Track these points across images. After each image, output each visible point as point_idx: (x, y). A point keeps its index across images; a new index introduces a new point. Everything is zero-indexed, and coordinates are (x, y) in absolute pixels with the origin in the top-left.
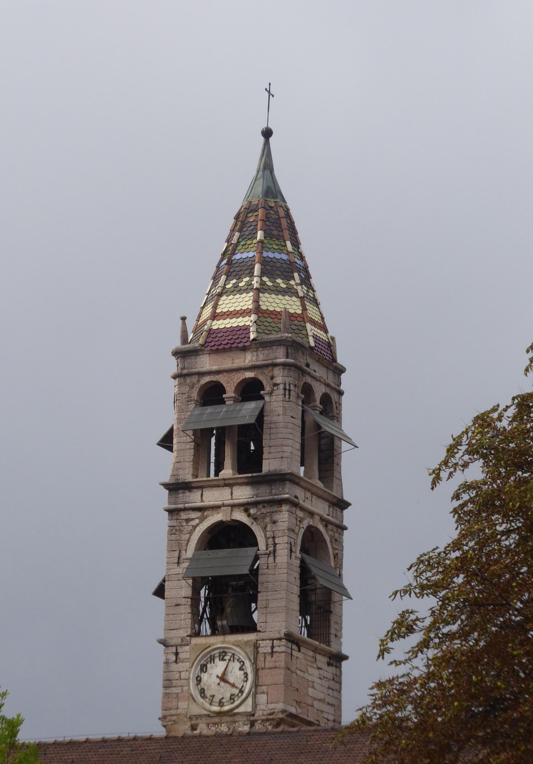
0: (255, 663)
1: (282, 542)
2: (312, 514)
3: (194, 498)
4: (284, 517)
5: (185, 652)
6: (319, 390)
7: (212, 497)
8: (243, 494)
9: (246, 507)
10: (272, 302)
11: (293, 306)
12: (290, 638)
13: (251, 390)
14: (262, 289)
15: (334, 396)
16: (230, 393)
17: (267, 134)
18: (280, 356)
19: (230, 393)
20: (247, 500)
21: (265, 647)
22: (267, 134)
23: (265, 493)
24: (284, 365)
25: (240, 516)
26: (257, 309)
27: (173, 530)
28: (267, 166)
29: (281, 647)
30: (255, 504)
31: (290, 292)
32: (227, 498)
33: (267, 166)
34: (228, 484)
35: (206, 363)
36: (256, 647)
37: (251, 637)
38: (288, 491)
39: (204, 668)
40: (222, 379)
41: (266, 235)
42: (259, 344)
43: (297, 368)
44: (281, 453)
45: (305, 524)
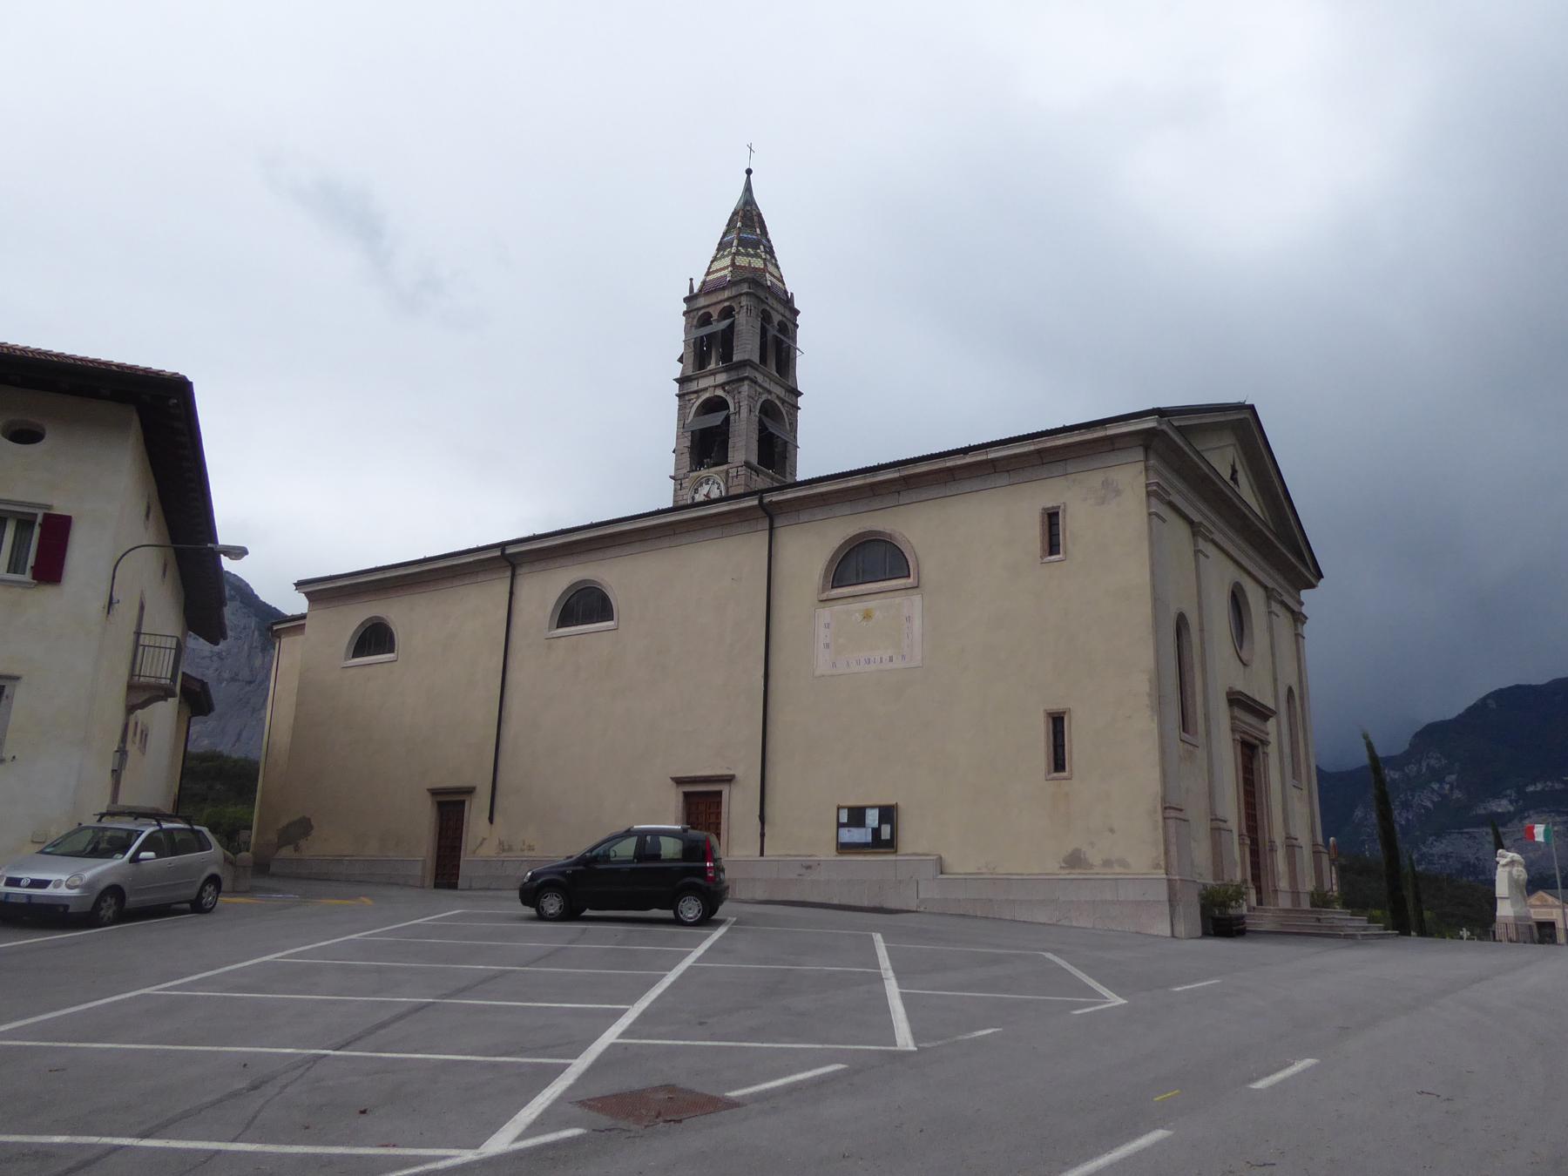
0: (726, 483)
1: (744, 404)
2: (770, 392)
3: (694, 386)
4: (745, 388)
5: (686, 483)
6: (776, 318)
7: (703, 383)
8: (721, 378)
9: (722, 386)
10: (742, 261)
11: (758, 263)
12: (747, 464)
13: (727, 313)
14: (737, 253)
15: (790, 326)
16: (715, 316)
17: (749, 172)
18: (745, 288)
19: (715, 316)
20: (1279, 839)
21: (733, 472)
22: (749, 172)
23: (734, 375)
24: (747, 294)
25: (720, 392)
26: (733, 264)
27: (681, 408)
28: (748, 189)
29: (742, 471)
30: (727, 383)
31: (757, 256)
32: (711, 383)
33: (748, 189)
34: (713, 373)
35: (702, 302)
36: (727, 472)
37: (725, 467)
38: (748, 372)
39: (696, 491)
40: (710, 310)
41: (747, 225)
42: (732, 284)
43: (758, 297)
44: (747, 347)
45: (764, 397)
